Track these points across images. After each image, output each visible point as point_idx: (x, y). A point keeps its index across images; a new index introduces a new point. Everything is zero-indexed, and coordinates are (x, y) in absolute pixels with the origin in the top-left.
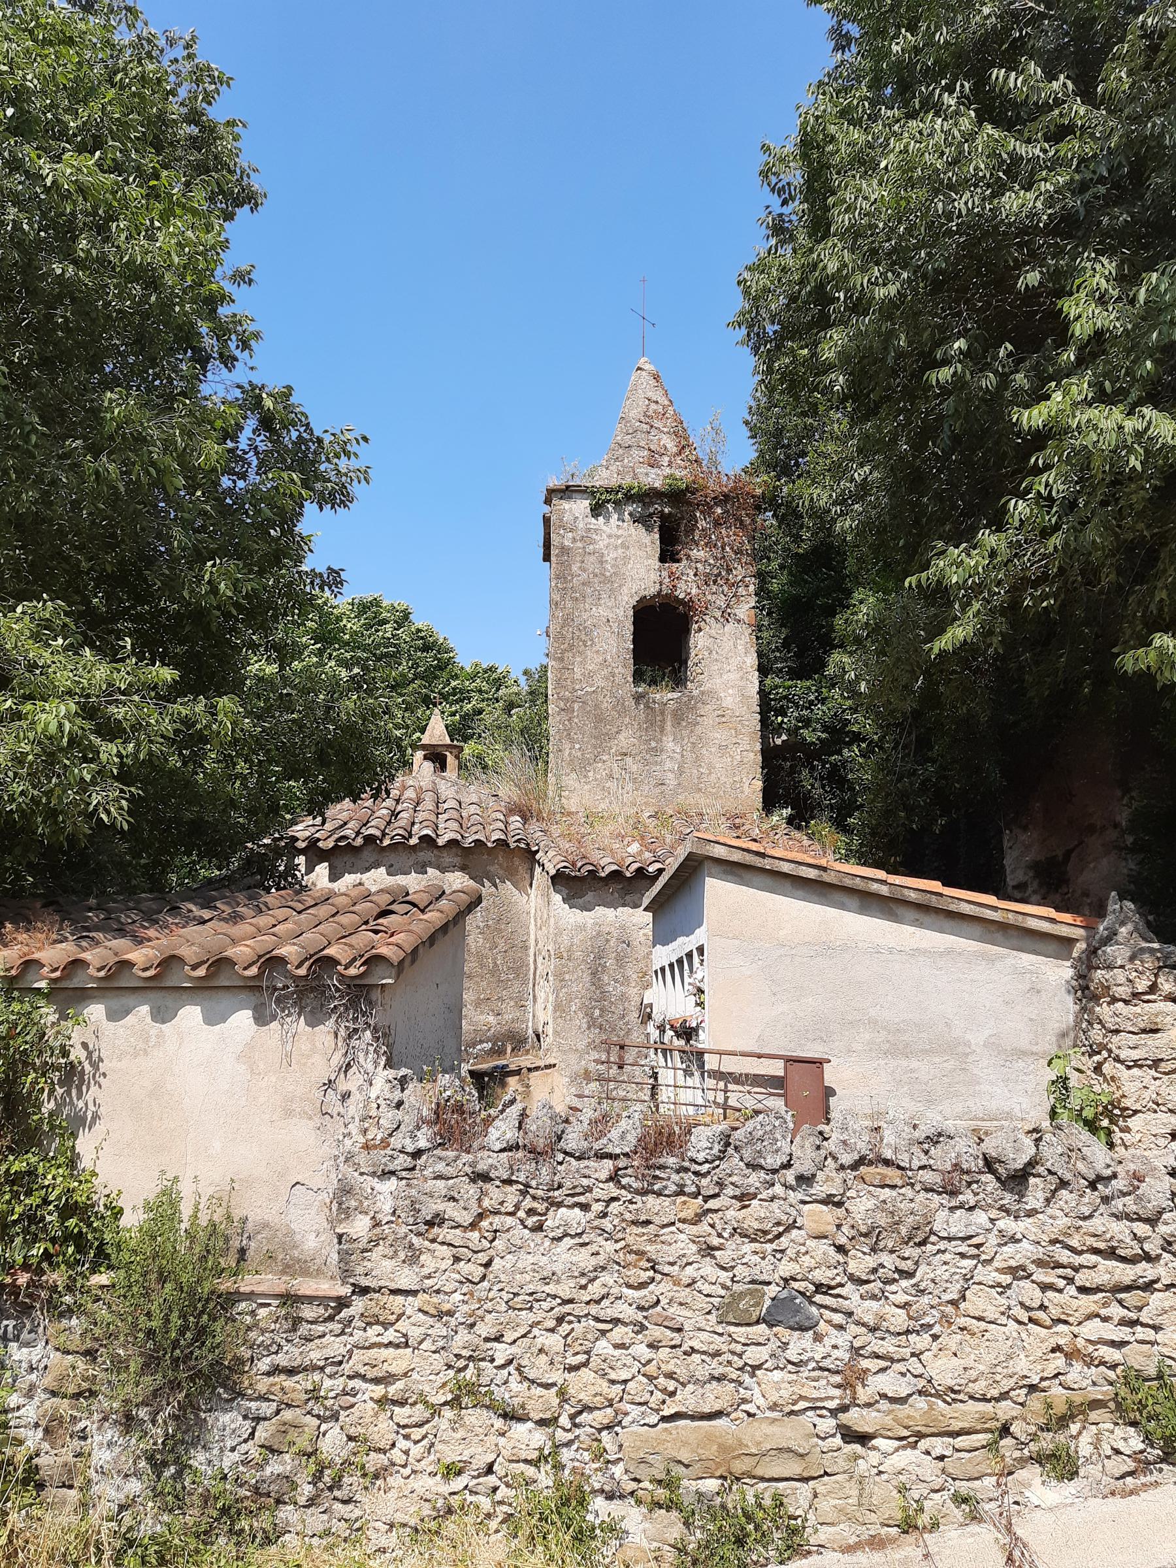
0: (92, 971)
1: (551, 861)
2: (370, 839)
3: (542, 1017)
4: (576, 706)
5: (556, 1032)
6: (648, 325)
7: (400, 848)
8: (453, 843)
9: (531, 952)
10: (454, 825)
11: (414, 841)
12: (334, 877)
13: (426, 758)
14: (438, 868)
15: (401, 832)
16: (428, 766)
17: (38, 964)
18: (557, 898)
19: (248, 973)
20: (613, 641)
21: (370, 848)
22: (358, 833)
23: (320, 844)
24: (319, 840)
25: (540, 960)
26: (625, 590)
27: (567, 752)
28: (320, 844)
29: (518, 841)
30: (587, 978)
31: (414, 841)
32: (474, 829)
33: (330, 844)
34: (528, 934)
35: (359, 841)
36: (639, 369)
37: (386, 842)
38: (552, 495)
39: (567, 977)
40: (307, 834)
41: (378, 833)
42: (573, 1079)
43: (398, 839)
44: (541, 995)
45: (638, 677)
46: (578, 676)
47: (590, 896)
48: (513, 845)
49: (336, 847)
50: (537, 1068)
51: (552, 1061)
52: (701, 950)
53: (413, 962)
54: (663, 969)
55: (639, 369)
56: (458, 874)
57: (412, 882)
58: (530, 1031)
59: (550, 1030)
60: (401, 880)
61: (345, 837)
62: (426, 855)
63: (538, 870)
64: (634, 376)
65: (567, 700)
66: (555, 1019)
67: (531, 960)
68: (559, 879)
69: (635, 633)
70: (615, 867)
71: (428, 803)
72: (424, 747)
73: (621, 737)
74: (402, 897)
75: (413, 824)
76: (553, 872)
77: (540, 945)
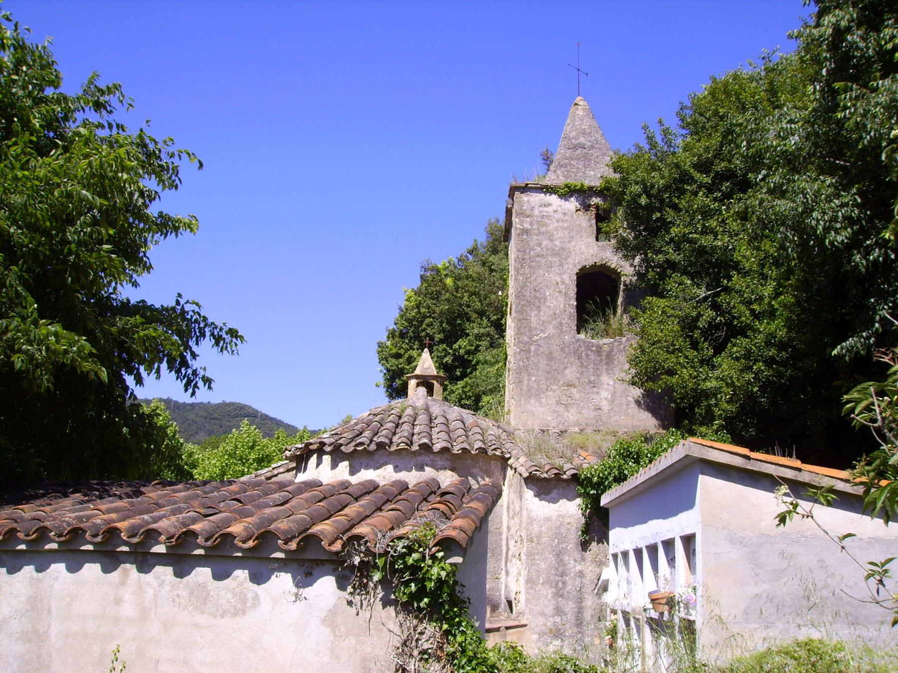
0: (200, 540)
1: (521, 463)
2: (380, 446)
3: (514, 588)
4: (533, 348)
5: (527, 600)
6: (582, 75)
7: (404, 452)
8: (445, 450)
9: (504, 536)
10: (443, 435)
11: (415, 448)
12: (353, 471)
13: (418, 385)
14: (433, 467)
15: (405, 440)
16: (422, 390)
17: (194, 534)
18: (529, 494)
19: (246, 546)
20: (561, 299)
21: (381, 452)
22: (371, 441)
23: (343, 448)
24: (341, 445)
25: (512, 543)
26: (570, 261)
27: (526, 382)
28: (343, 448)
29: (495, 449)
30: (552, 558)
31: (415, 448)
32: (460, 440)
33: (350, 448)
34: (501, 523)
35: (373, 447)
36: (576, 104)
37: (393, 448)
38: (513, 190)
39: (536, 557)
40: (332, 440)
41: (387, 441)
42: (541, 634)
43: (402, 446)
44: (513, 571)
45: (581, 325)
46: (534, 325)
47: (554, 494)
48: (490, 453)
49: (355, 450)
50: (824, 531)
51: (524, 622)
52: (689, 541)
53: (471, 544)
54: (625, 554)
55: (576, 104)
56: (450, 472)
57: (412, 477)
58: (503, 597)
59: (522, 597)
60: (403, 476)
61: (361, 444)
62: (426, 458)
63: (510, 472)
64: (573, 109)
65: (526, 343)
66: (527, 589)
67: (504, 543)
68: (532, 481)
69: (578, 293)
70: (574, 471)
71: (422, 418)
72: (417, 377)
73: (567, 372)
74: (403, 487)
75: (413, 434)
76: (526, 475)
77: (513, 531)
